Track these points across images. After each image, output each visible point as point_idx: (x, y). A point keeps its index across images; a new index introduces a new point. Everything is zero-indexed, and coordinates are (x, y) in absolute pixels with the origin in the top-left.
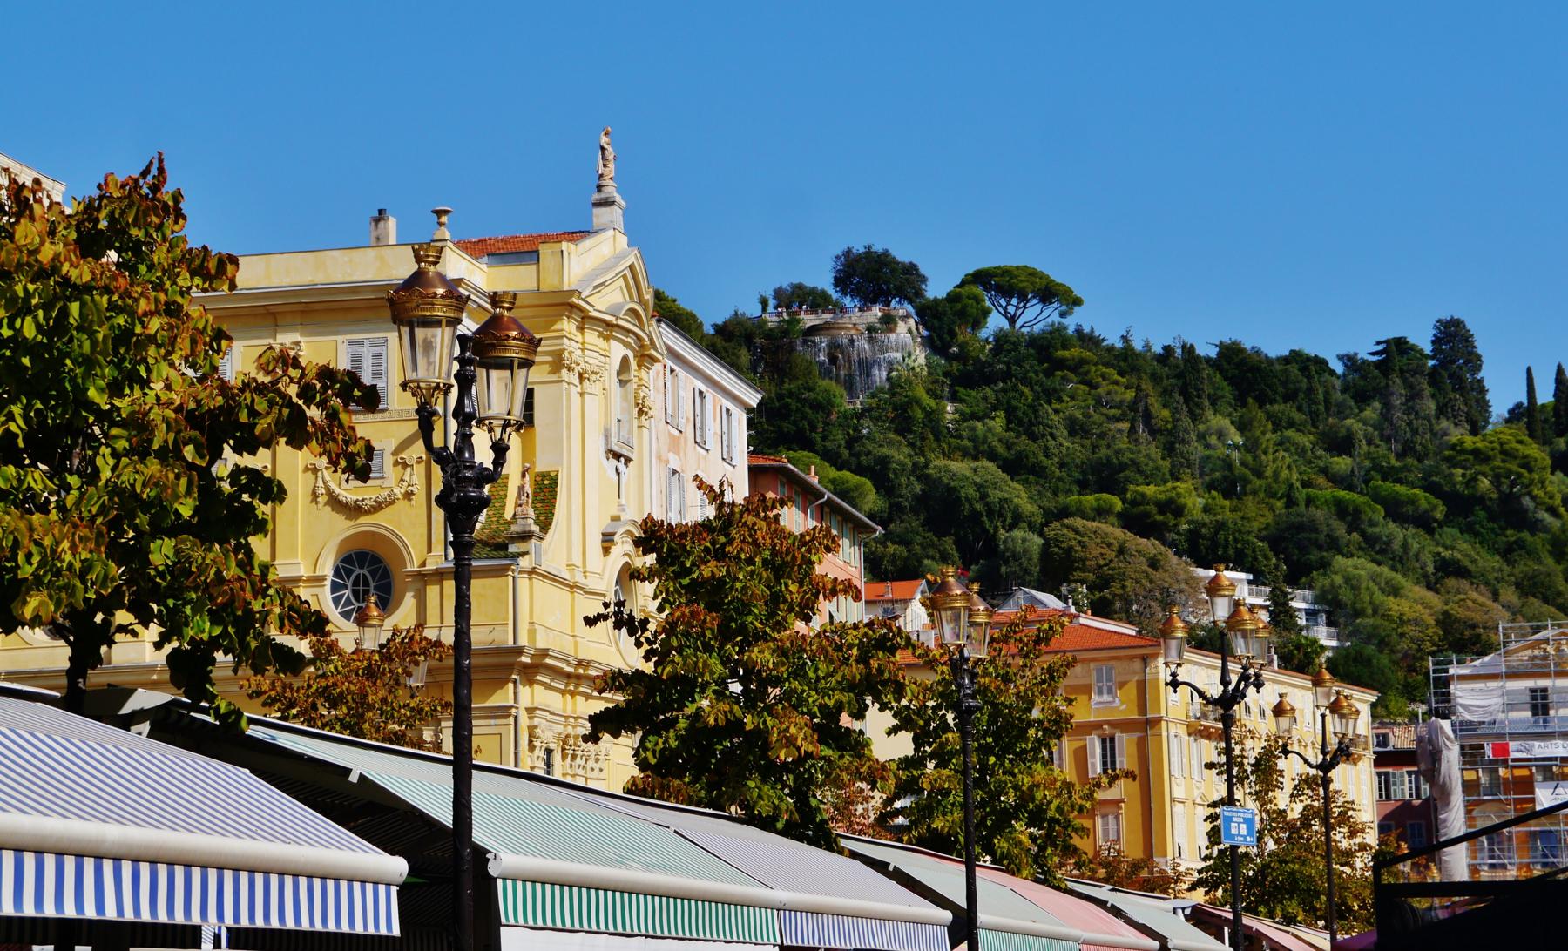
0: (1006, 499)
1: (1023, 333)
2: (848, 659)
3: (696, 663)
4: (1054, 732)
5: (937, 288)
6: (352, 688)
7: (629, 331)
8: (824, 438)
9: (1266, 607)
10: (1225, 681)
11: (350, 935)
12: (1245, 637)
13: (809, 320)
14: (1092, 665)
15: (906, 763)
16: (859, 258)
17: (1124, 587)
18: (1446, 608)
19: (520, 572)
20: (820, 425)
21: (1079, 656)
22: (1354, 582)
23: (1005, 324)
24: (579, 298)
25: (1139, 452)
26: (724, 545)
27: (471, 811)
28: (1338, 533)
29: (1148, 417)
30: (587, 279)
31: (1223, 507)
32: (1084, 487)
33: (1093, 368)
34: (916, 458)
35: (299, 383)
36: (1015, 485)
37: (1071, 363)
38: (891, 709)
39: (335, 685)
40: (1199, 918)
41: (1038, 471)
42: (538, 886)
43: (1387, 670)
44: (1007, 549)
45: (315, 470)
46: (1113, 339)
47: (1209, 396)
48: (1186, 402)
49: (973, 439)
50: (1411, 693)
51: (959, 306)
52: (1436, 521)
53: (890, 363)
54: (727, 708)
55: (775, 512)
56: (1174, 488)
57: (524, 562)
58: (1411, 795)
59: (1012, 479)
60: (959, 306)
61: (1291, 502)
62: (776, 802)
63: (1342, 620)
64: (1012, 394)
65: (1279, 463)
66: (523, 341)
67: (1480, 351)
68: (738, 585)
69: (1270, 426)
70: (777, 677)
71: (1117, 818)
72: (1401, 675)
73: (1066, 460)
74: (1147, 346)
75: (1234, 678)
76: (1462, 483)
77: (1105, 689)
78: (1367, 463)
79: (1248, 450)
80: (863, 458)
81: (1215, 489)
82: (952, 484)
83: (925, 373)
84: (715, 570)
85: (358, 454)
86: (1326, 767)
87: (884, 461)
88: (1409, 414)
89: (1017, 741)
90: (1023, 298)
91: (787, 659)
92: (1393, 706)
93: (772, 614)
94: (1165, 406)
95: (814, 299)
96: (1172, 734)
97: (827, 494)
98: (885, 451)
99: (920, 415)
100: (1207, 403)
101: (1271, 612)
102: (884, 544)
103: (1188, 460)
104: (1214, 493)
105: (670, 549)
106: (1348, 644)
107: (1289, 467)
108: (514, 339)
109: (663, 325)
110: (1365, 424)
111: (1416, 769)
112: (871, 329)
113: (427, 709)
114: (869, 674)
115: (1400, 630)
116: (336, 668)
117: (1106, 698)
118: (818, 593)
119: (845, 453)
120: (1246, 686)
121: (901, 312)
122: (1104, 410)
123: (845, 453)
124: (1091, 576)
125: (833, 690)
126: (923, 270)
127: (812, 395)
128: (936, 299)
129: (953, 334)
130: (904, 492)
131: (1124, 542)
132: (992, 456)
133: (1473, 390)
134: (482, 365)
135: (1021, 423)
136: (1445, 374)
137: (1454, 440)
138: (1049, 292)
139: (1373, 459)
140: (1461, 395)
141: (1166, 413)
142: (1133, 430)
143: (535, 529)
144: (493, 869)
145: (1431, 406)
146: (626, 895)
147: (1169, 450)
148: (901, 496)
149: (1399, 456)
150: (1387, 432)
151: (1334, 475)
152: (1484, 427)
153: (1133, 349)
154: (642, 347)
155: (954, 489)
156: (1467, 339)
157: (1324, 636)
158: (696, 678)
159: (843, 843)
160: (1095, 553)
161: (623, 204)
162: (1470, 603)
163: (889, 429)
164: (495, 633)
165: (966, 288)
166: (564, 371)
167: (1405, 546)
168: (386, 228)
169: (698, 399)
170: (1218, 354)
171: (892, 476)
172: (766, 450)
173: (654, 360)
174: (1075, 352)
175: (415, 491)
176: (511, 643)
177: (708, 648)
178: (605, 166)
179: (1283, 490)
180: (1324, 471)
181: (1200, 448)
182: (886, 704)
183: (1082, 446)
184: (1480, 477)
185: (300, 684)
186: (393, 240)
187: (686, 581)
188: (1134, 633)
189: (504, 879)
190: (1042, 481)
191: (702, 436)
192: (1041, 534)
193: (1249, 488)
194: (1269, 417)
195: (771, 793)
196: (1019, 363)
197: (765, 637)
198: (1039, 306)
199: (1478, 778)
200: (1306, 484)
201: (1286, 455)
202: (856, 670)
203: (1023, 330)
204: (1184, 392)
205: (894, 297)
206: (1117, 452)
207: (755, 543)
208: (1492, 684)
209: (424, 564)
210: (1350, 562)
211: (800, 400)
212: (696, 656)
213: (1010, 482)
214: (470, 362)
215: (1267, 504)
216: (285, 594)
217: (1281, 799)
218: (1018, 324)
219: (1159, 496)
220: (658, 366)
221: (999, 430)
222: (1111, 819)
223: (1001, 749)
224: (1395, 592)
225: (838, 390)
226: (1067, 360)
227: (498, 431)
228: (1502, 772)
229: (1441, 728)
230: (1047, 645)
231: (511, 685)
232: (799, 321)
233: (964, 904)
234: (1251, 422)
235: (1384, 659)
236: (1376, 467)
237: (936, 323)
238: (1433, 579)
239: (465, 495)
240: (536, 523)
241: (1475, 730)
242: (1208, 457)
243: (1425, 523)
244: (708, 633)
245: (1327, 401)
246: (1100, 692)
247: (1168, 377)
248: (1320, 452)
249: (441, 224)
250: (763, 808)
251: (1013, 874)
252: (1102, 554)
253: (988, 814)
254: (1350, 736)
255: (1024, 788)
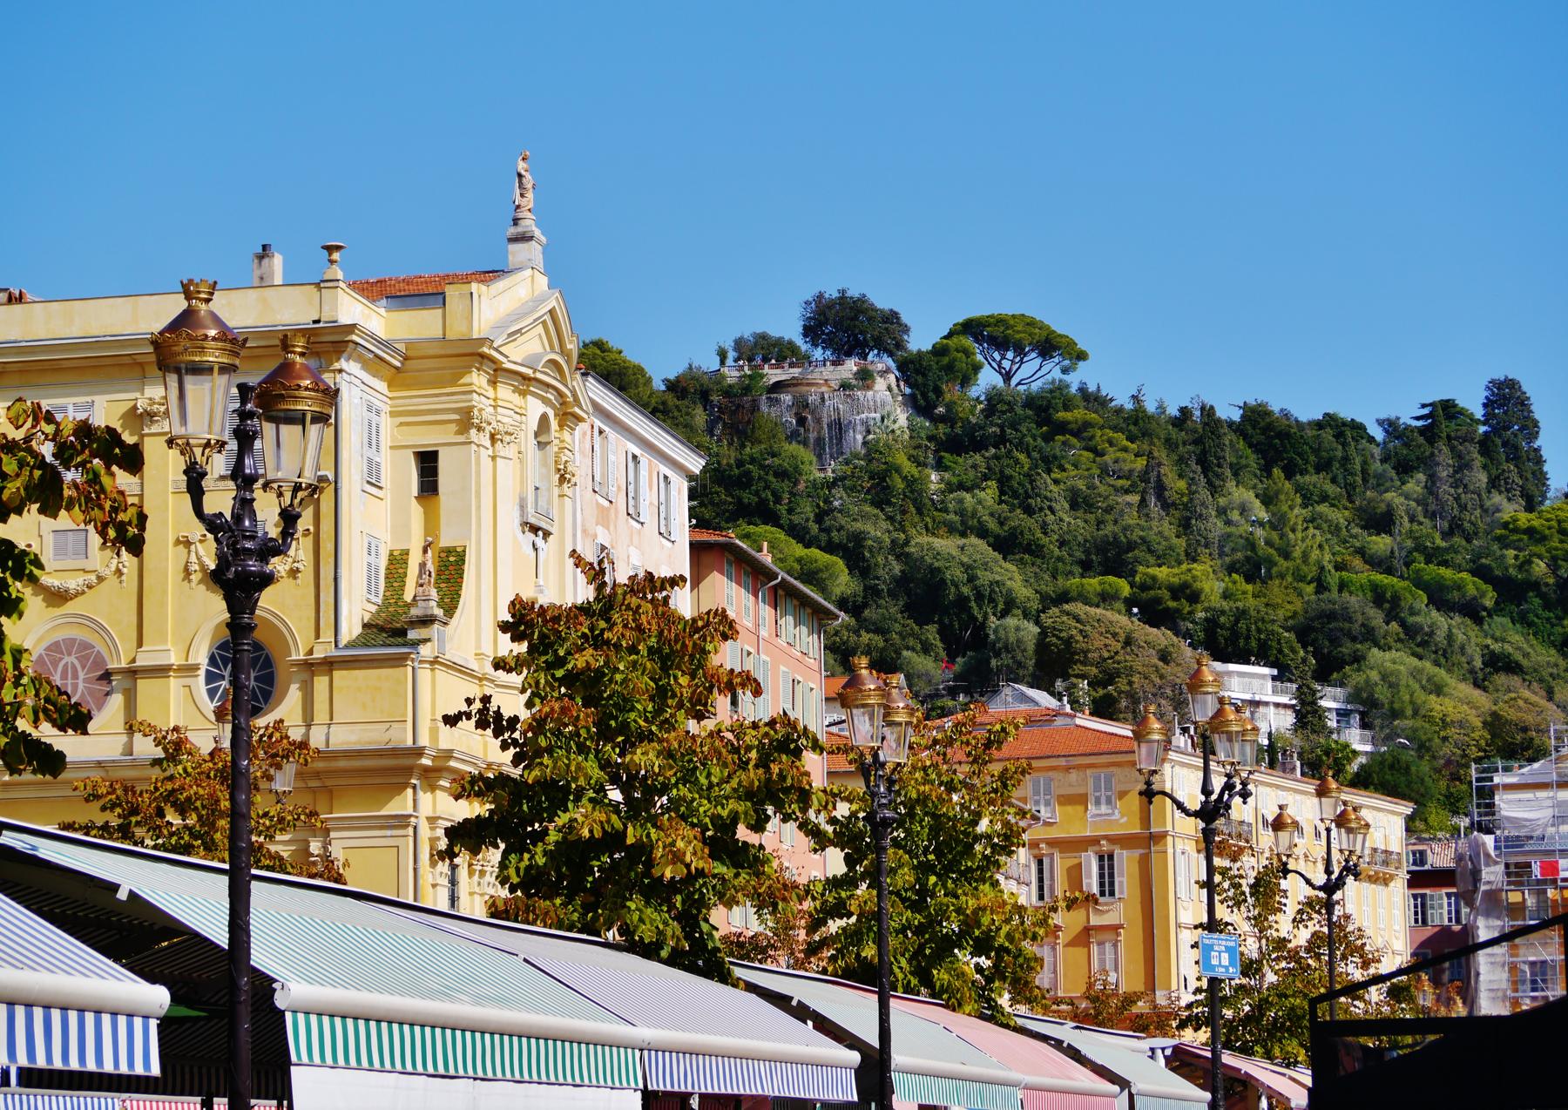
0: (997, 582)
1: (1019, 393)
2: (747, 763)
3: (568, 766)
4: (1003, 848)
5: (920, 340)
6: (201, 791)
7: (548, 385)
8: (790, 511)
9: (1293, 706)
10: (1206, 791)
11: (129, 1077)
12: (1230, 740)
13: (773, 375)
14: (1089, 772)
15: (834, 883)
16: (831, 304)
17: (1130, 683)
18: (1494, 708)
19: (421, 662)
20: (786, 495)
21: (1035, 764)
22: (1393, 679)
23: (998, 381)
24: (491, 347)
25: (1151, 528)
26: (603, 631)
27: (249, 936)
28: (1374, 623)
29: (1160, 489)
30: (498, 327)
31: (1244, 593)
32: (1086, 567)
33: (1099, 433)
34: (895, 535)
35: (53, 440)
36: (1008, 565)
37: (1073, 426)
38: (796, 820)
39: (182, 788)
40: (1181, 1062)
41: (1035, 550)
42: (338, 1021)
43: (1427, 779)
44: (999, 639)
45: (187, 543)
46: (1122, 399)
47: (1231, 466)
48: (1205, 472)
49: (961, 512)
50: (1454, 805)
51: (946, 360)
52: (1485, 609)
53: (865, 423)
54: (603, 818)
55: (664, 593)
56: (1189, 570)
57: (426, 651)
58: (1450, 920)
59: (1005, 559)
60: (946, 360)
61: (1321, 587)
62: (661, 927)
63: (1378, 722)
64: (1006, 462)
65: (1308, 542)
66: (317, 391)
67: (1537, 416)
68: (618, 677)
69: (1299, 500)
70: (663, 784)
71: (1115, 946)
72: (1443, 784)
73: (1067, 537)
74: (1161, 407)
75: (1218, 783)
76: (1514, 566)
77: (1103, 799)
78: (1409, 543)
79: (1274, 527)
80: (835, 533)
81: (1237, 572)
82: (936, 564)
83: (906, 437)
84: (591, 660)
85: (130, 523)
86: (1331, 887)
87: (858, 538)
88: (1457, 487)
89: (962, 858)
90: (1020, 351)
91: (675, 762)
92: (1433, 819)
93: (659, 711)
94: (1181, 476)
95: (781, 350)
96: (1178, 851)
97: (782, 575)
98: (859, 526)
99: (900, 485)
100: (1228, 473)
101: (1296, 712)
102: (857, 632)
103: (1205, 538)
104: (1234, 575)
105: (543, 636)
106: (1384, 749)
107: (1320, 546)
108: (307, 389)
109: (590, 379)
110: (1407, 498)
111: (1455, 890)
112: (845, 386)
113: (290, 818)
114: (769, 780)
115: (1442, 734)
116: (185, 770)
117: (1104, 809)
118: (712, 686)
119: (814, 528)
120: (1231, 796)
121: (880, 366)
122: (1111, 481)
123: (814, 528)
124: (1094, 671)
125: (727, 798)
126: (905, 318)
127: (777, 461)
128: (919, 351)
129: (938, 392)
130: (881, 572)
131: (1132, 631)
132: (983, 533)
133: (1529, 460)
134: (270, 419)
135: (1015, 495)
136: (1499, 442)
137: (1506, 517)
138: (1049, 345)
139: (1416, 539)
140: (1516, 466)
141: (1182, 485)
142: (1143, 503)
143: (439, 612)
144: (280, 1001)
145: (1483, 478)
146: (458, 1033)
147: (1185, 526)
148: (878, 578)
149: (1446, 535)
150: (1432, 507)
151: (1371, 557)
152: (1541, 503)
153: (1145, 411)
154: (563, 404)
155: (938, 570)
156: (1523, 403)
157: (1358, 741)
158: (568, 783)
159: (738, 972)
160: (1097, 644)
161: (543, 239)
162: (1521, 703)
163: (865, 501)
164: (391, 731)
165: (955, 339)
166: (473, 431)
167: (1450, 637)
168: (271, 266)
169: (631, 465)
170: (1242, 416)
171: (867, 554)
172: (723, 524)
173: (579, 419)
174: (1078, 414)
175: (302, 568)
176: (409, 743)
177: (582, 749)
178: (522, 195)
179: (1312, 572)
180: (1361, 552)
181: (1220, 524)
182: (790, 815)
183: (1086, 521)
184: (1536, 560)
185: (144, 788)
186: (278, 280)
187: (560, 673)
188: (1130, 734)
189: (294, 1012)
190: (1039, 561)
191: (636, 507)
192: (1037, 623)
193: (1275, 570)
194: (1299, 489)
195: (655, 915)
196: (1014, 426)
197: (650, 737)
198: (1039, 361)
199: (1524, 899)
200: (1339, 567)
201: (1317, 532)
202: (754, 776)
203: (1020, 387)
204: (1202, 461)
205: (871, 349)
206: (1125, 529)
207: (639, 629)
208: (1542, 794)
209: (311, 652)
210: (1387, 655)
211: (762, 467)
212: (569, 759)
213: (1002, 562)
214: (251, 415)
215: (1295, 589)
216: (41, 684)
217: (1283, 925)
218: (1014, 381)
219: (1172, 580)
220: (582, 428)
221: (990, 502)
222: (1108, 946)
223: (944, 867)
224: (1438, 690)
225: (806, 455)
226: (1069, 423)
227: (288, 496)
228: (1551, 893)
229: (1484, 844)
230: (999, 749)
231: (410, 791)
232: (762, 376)
233: (876, 1043)
234: (1277, 493)
235: (1425, 767)
236: (1419, 548)
237: (920, 379)
238: (1480, 675)
239: (244, 571)
240: (439, 606)
241: (1522, 846)
242: (1229, 535)
243: (1472, 611)
244: (583, 732)
245: (1364, 472)
246: (1098, 802)
247: (1184, 444)
248: (1356, 530)
249: (332, 262)
250: (646, 933)
251: (954, 1010)
252: (1106, 645)
253: (927, 942)
254: (1358, 853)
255: (968, 912)
